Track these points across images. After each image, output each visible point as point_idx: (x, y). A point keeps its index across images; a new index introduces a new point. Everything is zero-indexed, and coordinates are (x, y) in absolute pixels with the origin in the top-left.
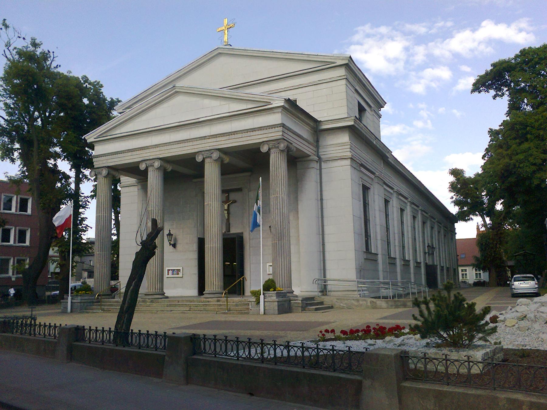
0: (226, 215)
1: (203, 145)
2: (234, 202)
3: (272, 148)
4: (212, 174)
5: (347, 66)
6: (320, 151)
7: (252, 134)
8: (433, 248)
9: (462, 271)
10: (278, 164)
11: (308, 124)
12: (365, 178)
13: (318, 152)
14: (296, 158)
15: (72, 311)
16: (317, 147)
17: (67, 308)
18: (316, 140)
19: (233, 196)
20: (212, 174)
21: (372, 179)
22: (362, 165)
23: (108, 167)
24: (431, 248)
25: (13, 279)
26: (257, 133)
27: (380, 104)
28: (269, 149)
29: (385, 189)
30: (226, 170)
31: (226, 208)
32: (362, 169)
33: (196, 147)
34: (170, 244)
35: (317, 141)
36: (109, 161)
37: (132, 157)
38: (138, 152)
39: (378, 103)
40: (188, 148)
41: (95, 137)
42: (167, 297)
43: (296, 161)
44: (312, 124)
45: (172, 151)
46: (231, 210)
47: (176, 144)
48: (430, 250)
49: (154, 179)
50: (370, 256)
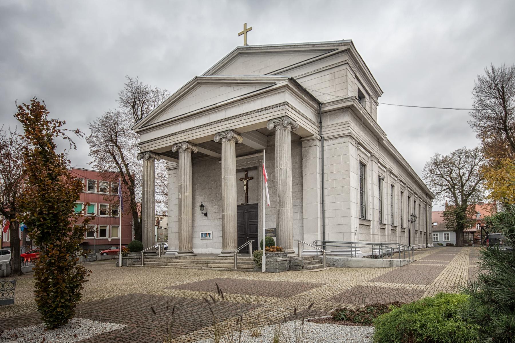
0: (245, 189)
1: (220, 128)
2: (252, 178)
3: (277, 125)
4: (229, 152)
5: (348, 51)
6: (323, 130)
7: (260, 113)
8: (415, 217)
9: (434, 235)
10: (284, 142)
11: (312, 107)
12: (362, 155)
13: (320, 132)
14: (301, 138)
15: (122, 265)
16: (320, 127)
17: (118, 262)
18: (319, 121)
19: (250, 174)
20: (229, 152)
21: (369, 157)
22: (359, 143)
23: (151, 152)
24: (414, 216)
25: (110, 240)
26: (264, 112)
27: (377, 93)
28: (275, 127)
29: (379, 167)
30: (241, 152)
31: (245, 183)
32: (360, 147)
33: (214, 129)
34: (202, 213)
35: (320, 122)
36: (150, 146)
37: (166, 142)
38: (171, 138)
39: (376, 91)
40: (208, 131)
41: (139, 127)
42: (196, 255)
43: (299, 141)
44: (315, 106)
45: (196, 134)
46: (249, 186)
47: (200, 130)
48: (413, 218)
49: (185, 160)
50: (364, 223)
